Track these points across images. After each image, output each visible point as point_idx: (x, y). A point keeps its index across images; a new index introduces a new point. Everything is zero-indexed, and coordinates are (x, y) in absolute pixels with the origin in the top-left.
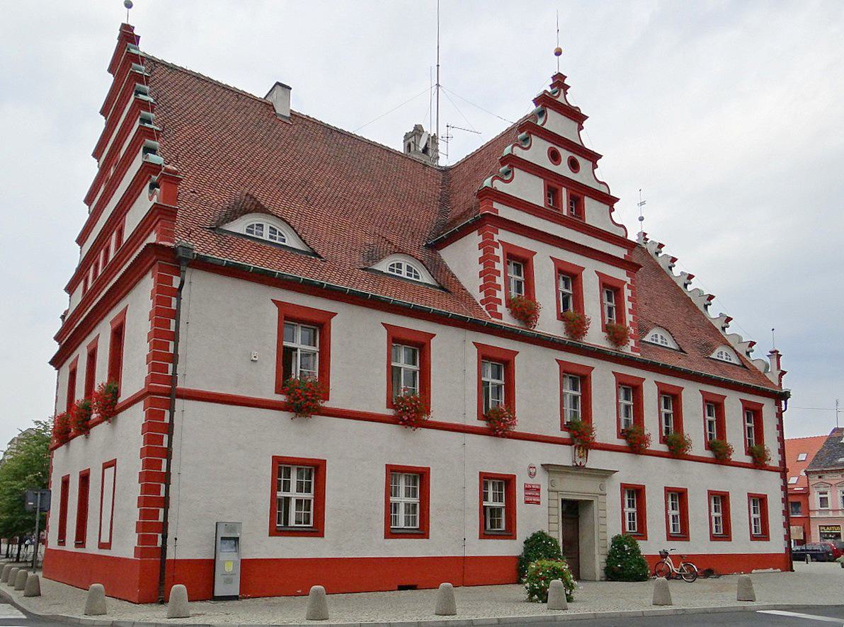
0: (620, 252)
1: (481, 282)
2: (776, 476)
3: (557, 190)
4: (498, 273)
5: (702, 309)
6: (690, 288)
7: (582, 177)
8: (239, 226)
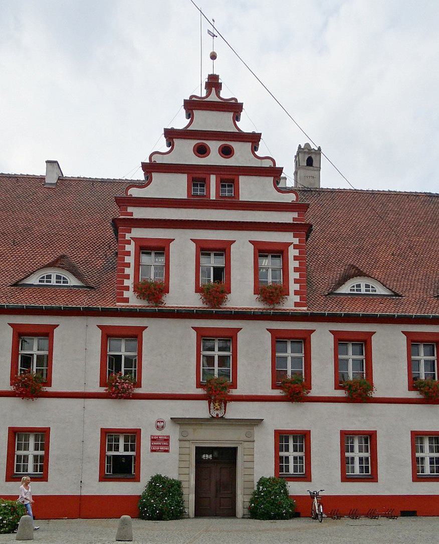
8: (345, 289)
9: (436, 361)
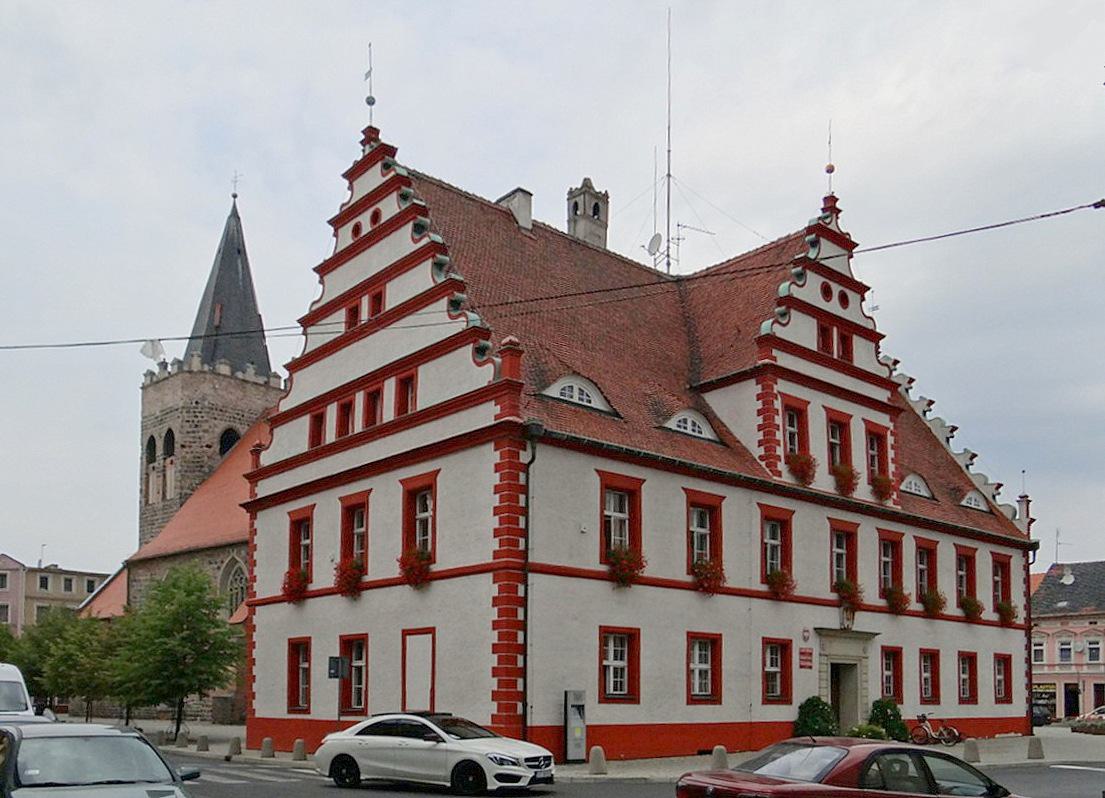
0: (882, 395)
1: (760, 436)
3: (848, 338)
5: (944, 442)
7: (848, 314)
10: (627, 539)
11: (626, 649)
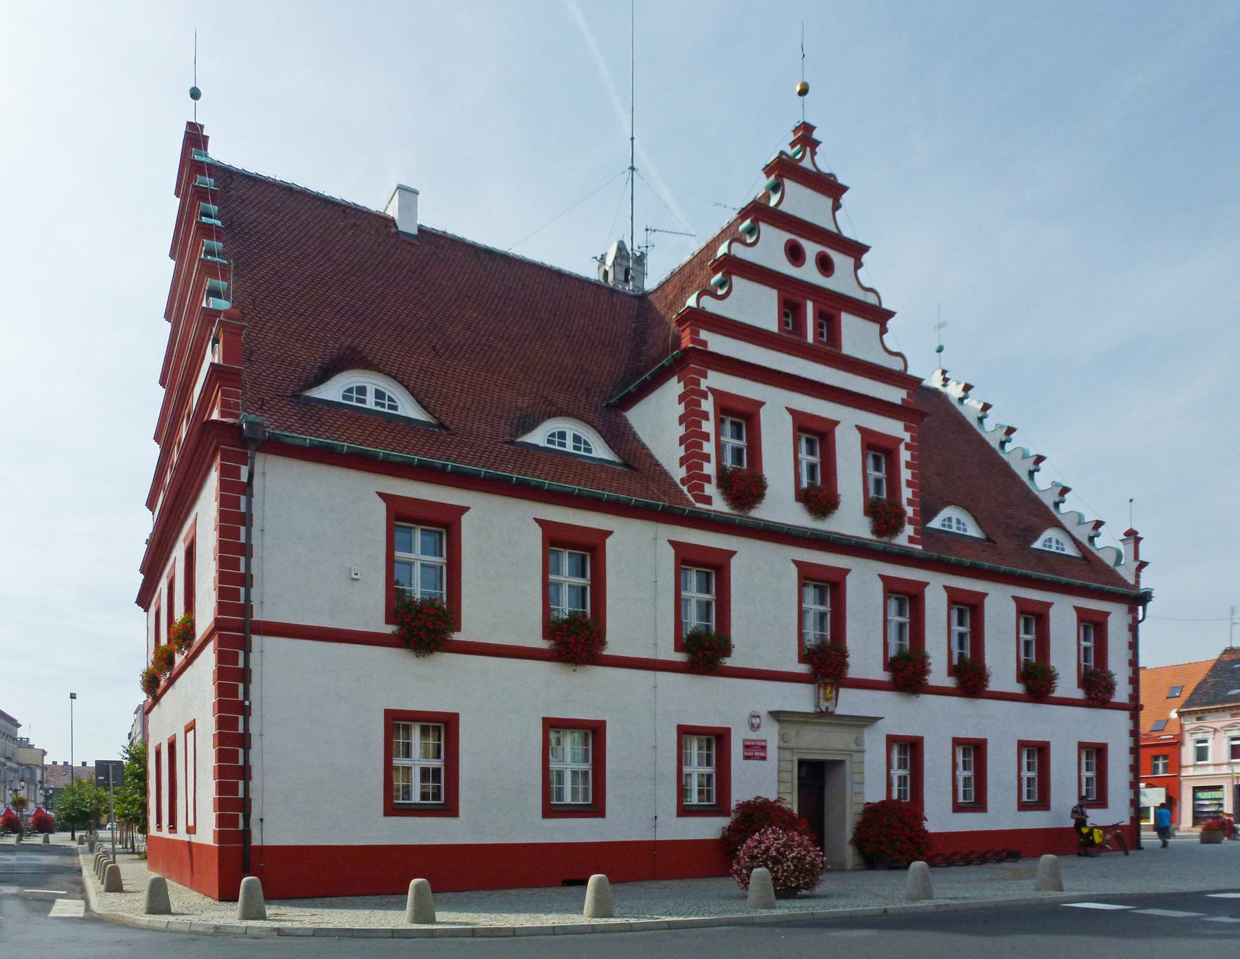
0: (895, 395)
1: (681, 452)
2: (1124, 716)
4: (706, 437)
5: (1024, 477)
6: (1008, 447)
7: (840, 282)
8: (332, 391)
9: (589, 589)
10: (828, 634)
11: (908, 757)
